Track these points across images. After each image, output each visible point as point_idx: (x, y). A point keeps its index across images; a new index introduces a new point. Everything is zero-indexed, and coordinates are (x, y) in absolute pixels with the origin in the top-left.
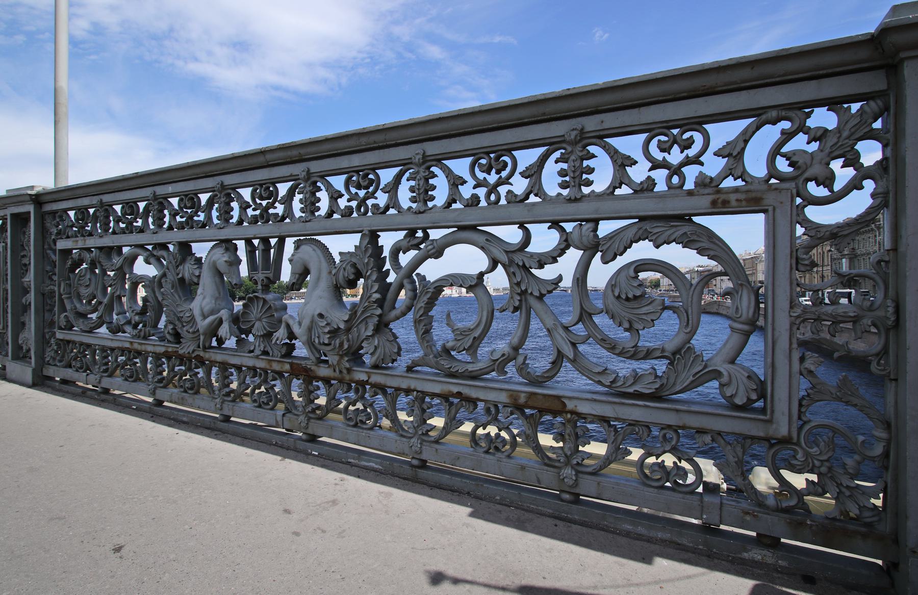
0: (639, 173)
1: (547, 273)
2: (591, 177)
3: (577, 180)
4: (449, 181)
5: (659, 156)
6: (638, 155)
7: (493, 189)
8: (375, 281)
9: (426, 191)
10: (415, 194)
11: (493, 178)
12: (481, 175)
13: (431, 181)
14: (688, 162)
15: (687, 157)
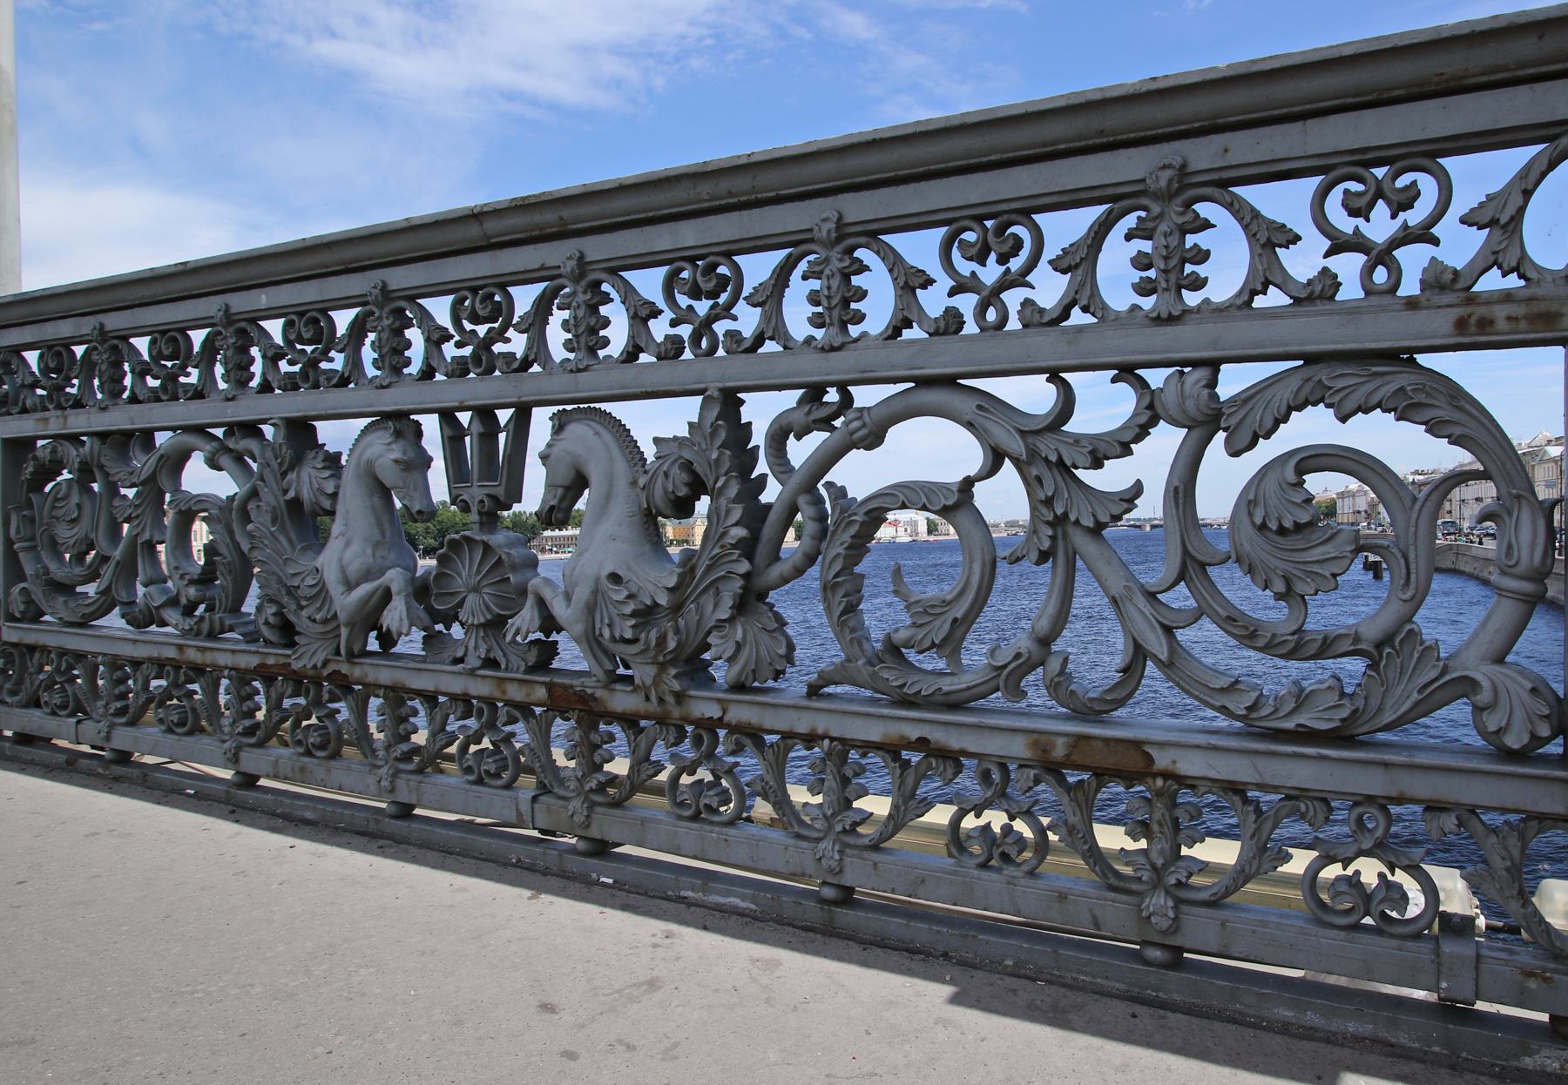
0: (1302, 262)
1: (1110, 478)
2: (1202, 270)
3: (1173, 277)
4: (895, 279)
5: (1345, 224)
6: (1302, 223)
7: (992, 297)
8: (734, 501)
9: (846, 302)
10: (820, 309)
11: (990, 273)
12: (964, 267)
13: (856, 280)
14: (1407, 237)
15: (1405, 226)
